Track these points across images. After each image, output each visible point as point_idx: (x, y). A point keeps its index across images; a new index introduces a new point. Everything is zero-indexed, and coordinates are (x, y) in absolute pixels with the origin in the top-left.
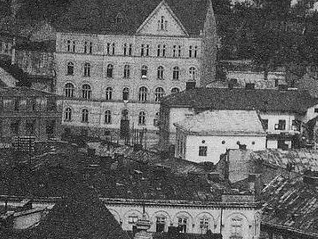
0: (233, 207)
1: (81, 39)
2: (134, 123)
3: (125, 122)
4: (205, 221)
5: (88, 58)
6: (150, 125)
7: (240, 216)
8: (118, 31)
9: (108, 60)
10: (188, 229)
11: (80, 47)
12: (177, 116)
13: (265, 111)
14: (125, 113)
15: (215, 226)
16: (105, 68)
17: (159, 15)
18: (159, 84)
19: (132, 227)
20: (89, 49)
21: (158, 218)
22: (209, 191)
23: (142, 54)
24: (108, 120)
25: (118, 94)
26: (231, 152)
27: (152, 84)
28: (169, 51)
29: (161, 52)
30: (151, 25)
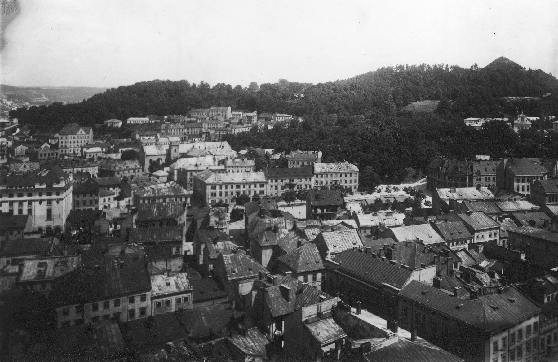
0: (92, 166)
1: (64, 137)
3: (74, 152)
5: (66, 140)
6: (79, 152)
8: (73, 134)
10: (465, 230)
11: (72, 138)
12: (84, 150)
14: (74, 150)
19: (187, 243)
24: (70, 151)
25: (72, 146)
27: (80, 144)
30: (79, 133)
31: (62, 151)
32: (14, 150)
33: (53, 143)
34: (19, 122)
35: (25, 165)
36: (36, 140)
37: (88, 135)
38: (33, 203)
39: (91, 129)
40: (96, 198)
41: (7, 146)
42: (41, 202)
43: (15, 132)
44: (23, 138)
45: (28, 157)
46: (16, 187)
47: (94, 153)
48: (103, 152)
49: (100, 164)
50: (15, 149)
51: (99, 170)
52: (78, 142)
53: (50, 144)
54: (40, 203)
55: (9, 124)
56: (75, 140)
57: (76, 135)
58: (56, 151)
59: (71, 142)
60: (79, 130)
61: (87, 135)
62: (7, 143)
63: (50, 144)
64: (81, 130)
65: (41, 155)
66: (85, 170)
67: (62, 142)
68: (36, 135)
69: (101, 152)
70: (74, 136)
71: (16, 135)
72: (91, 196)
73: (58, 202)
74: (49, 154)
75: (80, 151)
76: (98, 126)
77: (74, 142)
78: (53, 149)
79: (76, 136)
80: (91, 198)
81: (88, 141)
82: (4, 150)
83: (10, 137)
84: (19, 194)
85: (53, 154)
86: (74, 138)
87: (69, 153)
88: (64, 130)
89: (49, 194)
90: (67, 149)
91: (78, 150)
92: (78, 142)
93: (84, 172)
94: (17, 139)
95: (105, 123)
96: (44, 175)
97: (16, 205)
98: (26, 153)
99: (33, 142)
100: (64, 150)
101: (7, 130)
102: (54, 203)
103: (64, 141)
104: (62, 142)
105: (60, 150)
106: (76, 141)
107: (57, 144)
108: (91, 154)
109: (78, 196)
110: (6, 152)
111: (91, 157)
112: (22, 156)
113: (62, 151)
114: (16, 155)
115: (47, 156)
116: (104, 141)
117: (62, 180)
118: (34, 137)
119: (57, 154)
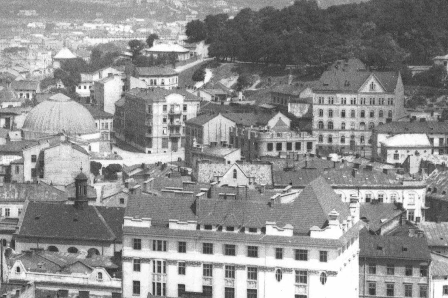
1: (326, 98)
2: (358, 142)
3: (352, 142)
4: (394, 195)
6: (366, 143)
7: (414, 193)
8: (348, 92)
9: (341, 108)
11: (326, 101)
12: (382, 138)
13: (432, 134)
14: (353, 137)
15: (399, 198)
16: (340, 111)
17: (370, 83)
18: (320, 119)
20: (331, 102)
21: (366, 195)
22: (396, 179)
23: (320, 102)
24: (343, 140)
25: (348, 127)
26: (411, 157)
27: (367, 120)
28: (376, 102)
29: (372, 102)
30: (366, 88)
31: (321, 139)
32: (201, 128)
33: (298, 115)
34: (210, 54)
35: (235, 171)
36: (253, 103)
37: (390, 96)
38: (260, 274)
39: (399, 80)
40: (423, 281)
41: (185, 117)
42: (279, 275)
43: (202, 79)
44: (220, 95)
45: (237, 147)
46: (220, 228)
47: (408, 148)
48: (433, 149)
49: (428, 181)
50: (206, 127)
51: (428, 200)
52: (363, 115)
53: (290, 116)
54: (279, 277)
55: (187, 57)
56: (354, 107)
57: (356, 92)
58: (307, 138)
59: (343, 115)
60: (363, 82)
61: (387, 97)
62: (185, 109)
63: (290, 116)
64: (372, 80)
65: (270, 147)
66: (388, 196)
67: (321, 113)
68: (253, 88)
69: (427, 147)
70: (354, 96)
71: (205, 87)
72: (409, 273)
73: (323, 281)
74: (289, 146)
75: (370, 141)
76: (416, 69)
77: (353, 114)
78: (297, 132)
79: (358, 97)
80: (407, 280)
81: (390, 114)
82: (178, 128)
83: (190, 91)
84: (297, 251)
85: (298, 146)
86: (353, 102)
87: (340, 144)
88: (326, 77)
89: (159, 246)
90: (334, 135)
91: (362, 139)
92: (363, 115)
93: (387, 200)
94: (207, 97)
95: (437, 63)
96: (287, 200)
97: (219, 274)
98: (232, 137)
99: (247, 109)
100: (326, 134)
101: (182, 72)
102: (314, 280)
103: (326, 108)
104: (321, 113)
105: (316, 133)
106: (357, 109)
107: (308, 119)
108: (400, 152)
109: (373, 271)
110: (181, 131)
111: (401, 161)
112: (224, 145)
113: (321, 139)
114: (206, 141)
115: (284, 149)
116: (436, 114)
117: (334, 218)
118: (247, 94)
119: (309, 145)
